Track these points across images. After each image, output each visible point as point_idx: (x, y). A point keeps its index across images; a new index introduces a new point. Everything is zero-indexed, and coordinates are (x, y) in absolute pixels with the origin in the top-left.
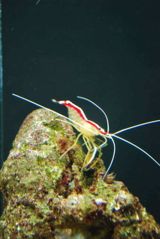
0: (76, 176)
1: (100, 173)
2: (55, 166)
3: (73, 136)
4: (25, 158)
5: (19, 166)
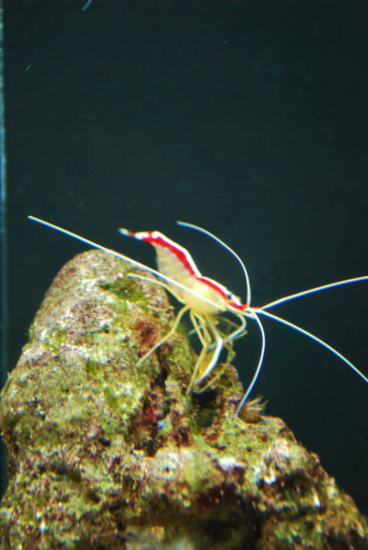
0: (175, 405)
1: (231, 398)
2: (126, 382)
3: (168, 312)
4: (59, 363)
5: (43, 382)
